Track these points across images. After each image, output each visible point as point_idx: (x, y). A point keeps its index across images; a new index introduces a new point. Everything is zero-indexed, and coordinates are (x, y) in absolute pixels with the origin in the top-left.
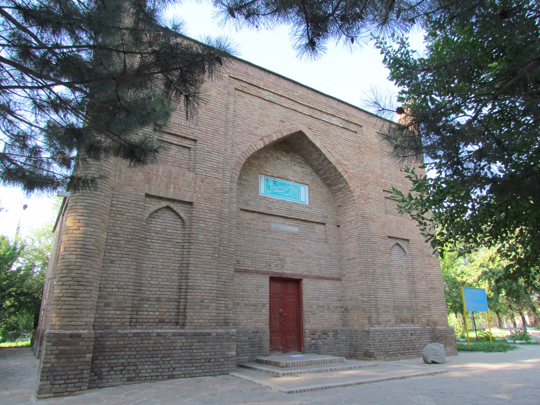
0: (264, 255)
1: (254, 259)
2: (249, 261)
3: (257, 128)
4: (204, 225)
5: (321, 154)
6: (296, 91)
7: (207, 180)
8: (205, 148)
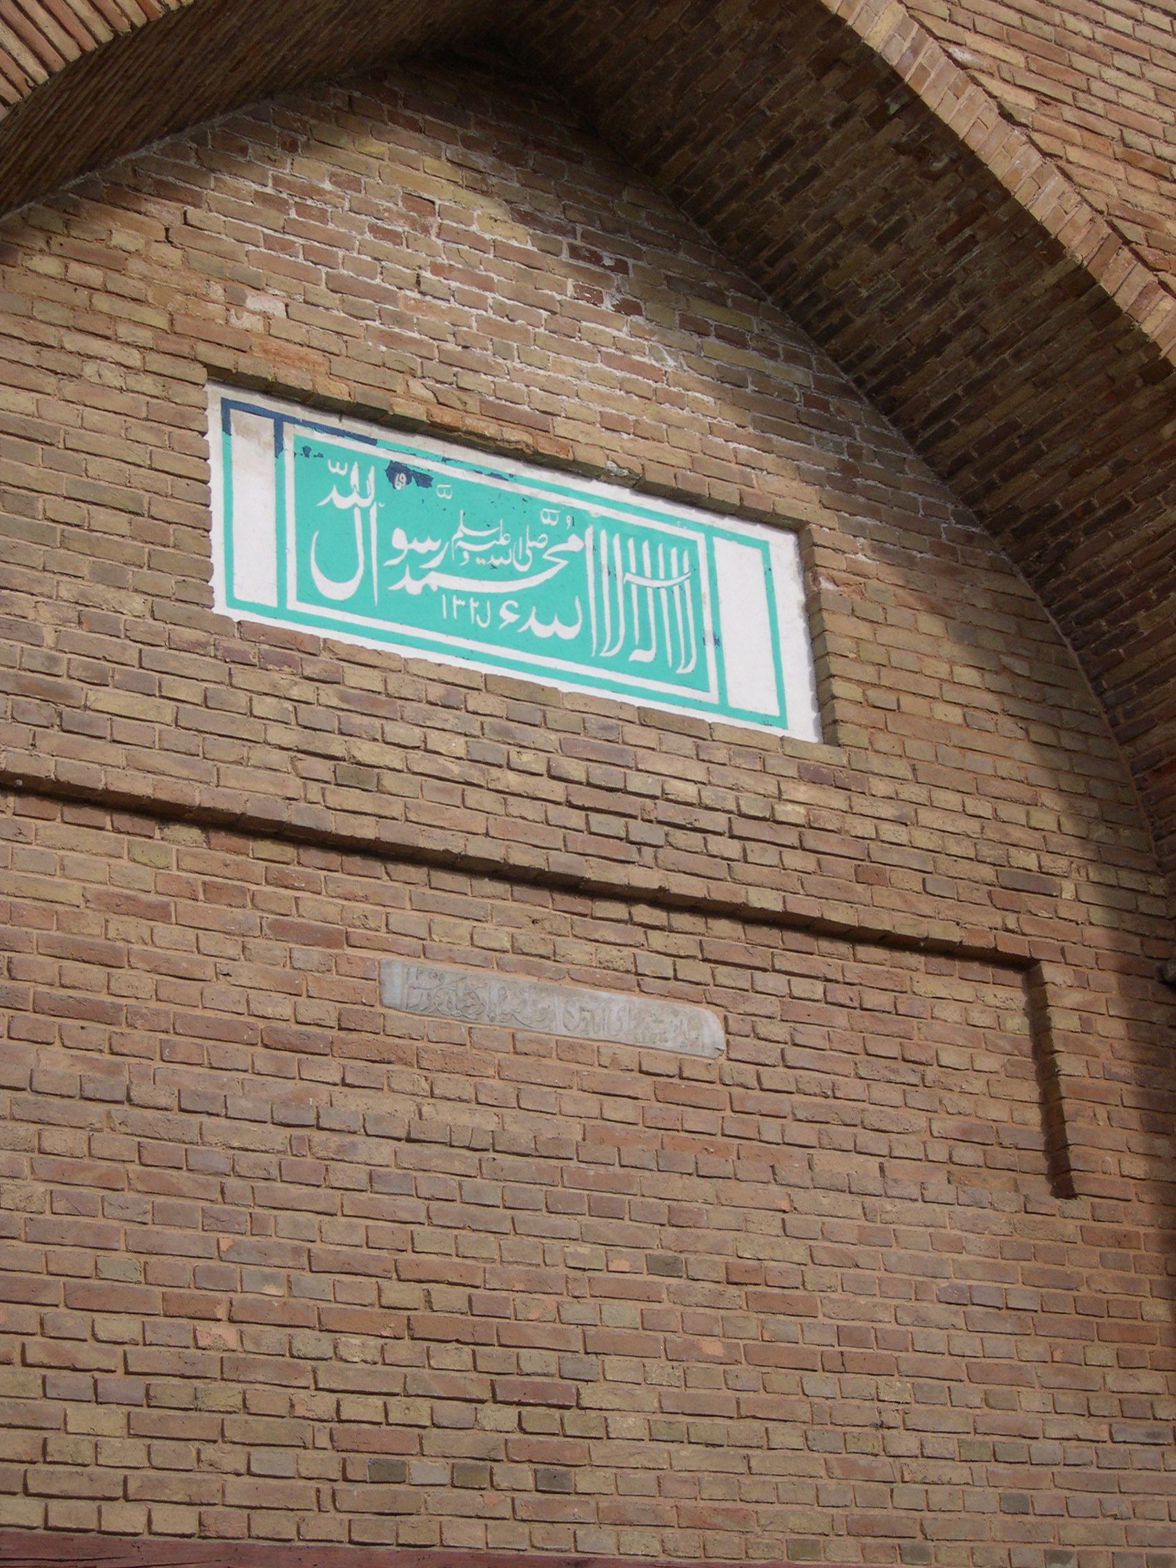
0: (308, 1342)
2: (109, 1420)
5: (931, 135)
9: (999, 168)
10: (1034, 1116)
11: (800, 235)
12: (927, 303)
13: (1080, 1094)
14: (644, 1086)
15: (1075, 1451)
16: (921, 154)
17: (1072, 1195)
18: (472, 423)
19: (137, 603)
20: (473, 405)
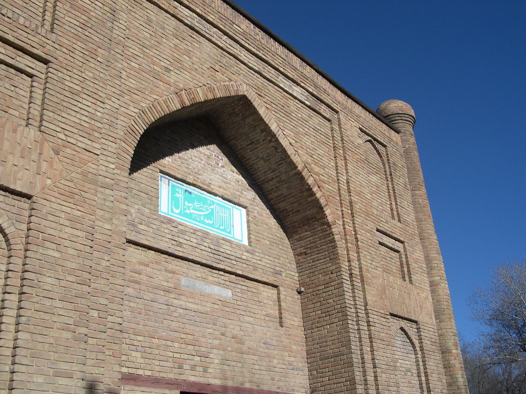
0: (169, 343)
1: (148, 350)
2: (138, 355)
3: (168, 70)
4: (57, 255)
5: (278, 146)
6: (237, 22)
7: (68, 151)
8: (67, 83)
9: (289, 152)
10: (277, 312)
11: (252, 158)
12: (271, 172)
13: (284, 309)
14: (219, 303)
15: (281, 370)
16: (276, 149)
17: (282, 327)
18: (199, 184)
19: (147, 211)
20: (199, 181)
